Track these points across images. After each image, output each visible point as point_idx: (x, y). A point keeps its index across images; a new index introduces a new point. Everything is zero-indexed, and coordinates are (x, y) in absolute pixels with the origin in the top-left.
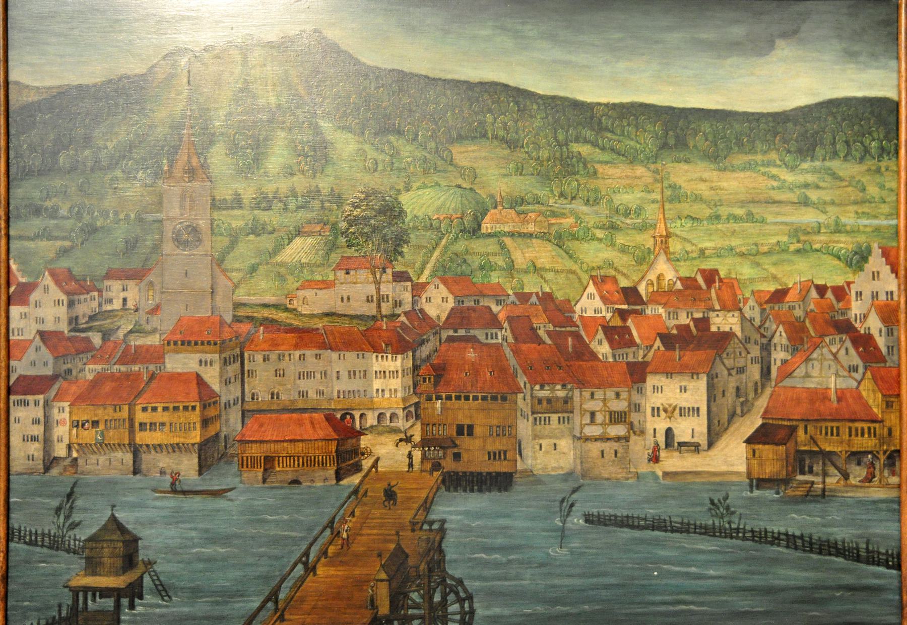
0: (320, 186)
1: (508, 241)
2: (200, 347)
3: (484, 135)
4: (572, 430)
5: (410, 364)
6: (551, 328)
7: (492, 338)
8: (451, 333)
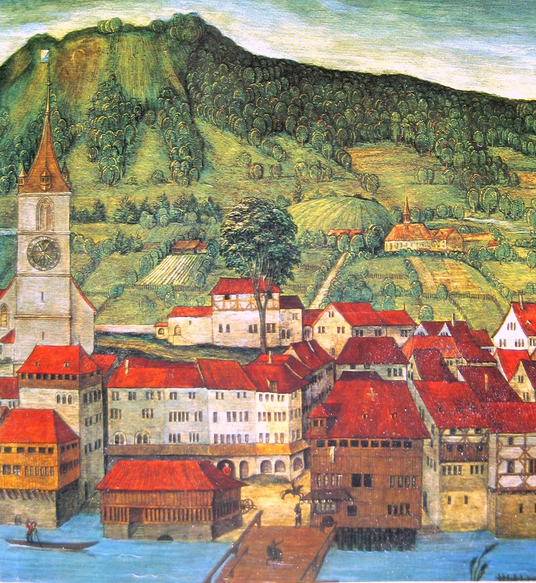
0: (196, 196)
1: (416, 261)
2: (57, 381)
3: (388, 137)
4: (486, 481)
5: (299, 404)
6: (465, 363)
7: (395, 375)
8: (348, 368)
